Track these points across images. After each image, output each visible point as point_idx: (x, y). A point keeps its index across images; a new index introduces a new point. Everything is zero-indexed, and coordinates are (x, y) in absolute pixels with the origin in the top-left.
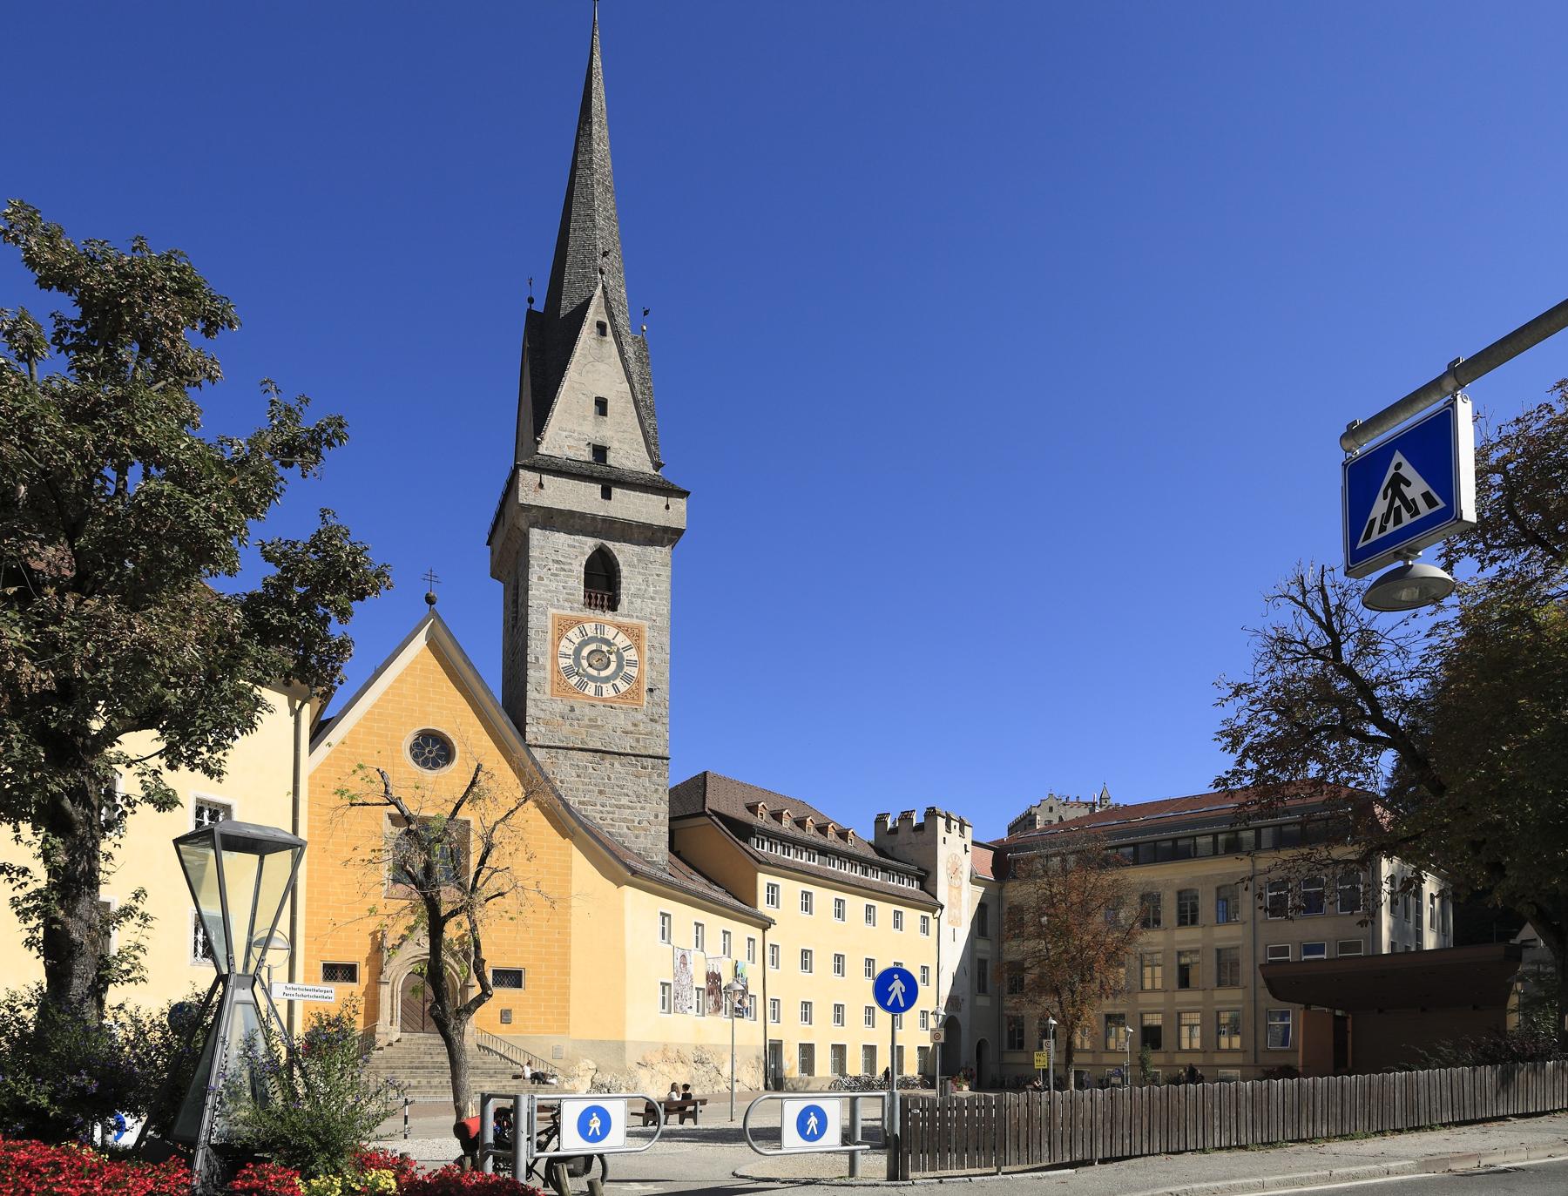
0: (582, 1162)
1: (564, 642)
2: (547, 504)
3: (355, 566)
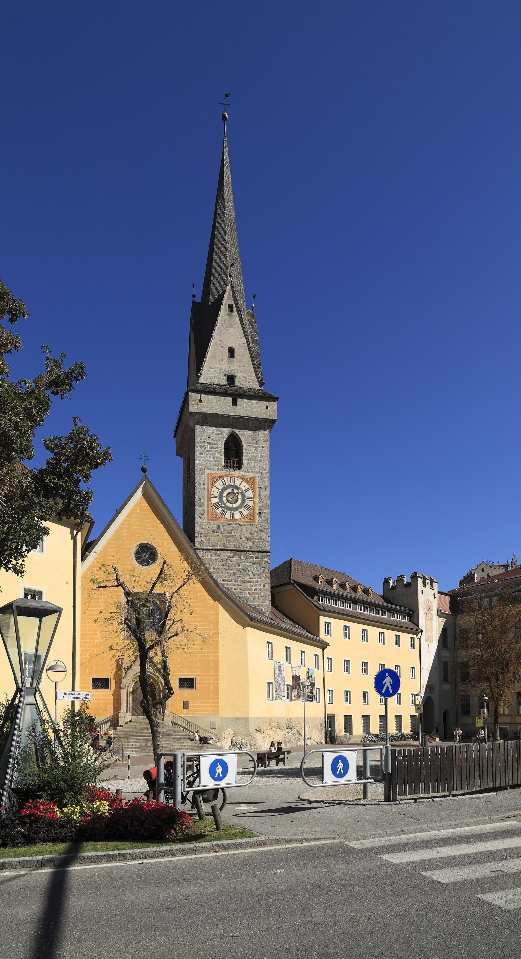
0: (212, 793)
1: (214, 489)
2: (204, 411)
3: (92, 449)
